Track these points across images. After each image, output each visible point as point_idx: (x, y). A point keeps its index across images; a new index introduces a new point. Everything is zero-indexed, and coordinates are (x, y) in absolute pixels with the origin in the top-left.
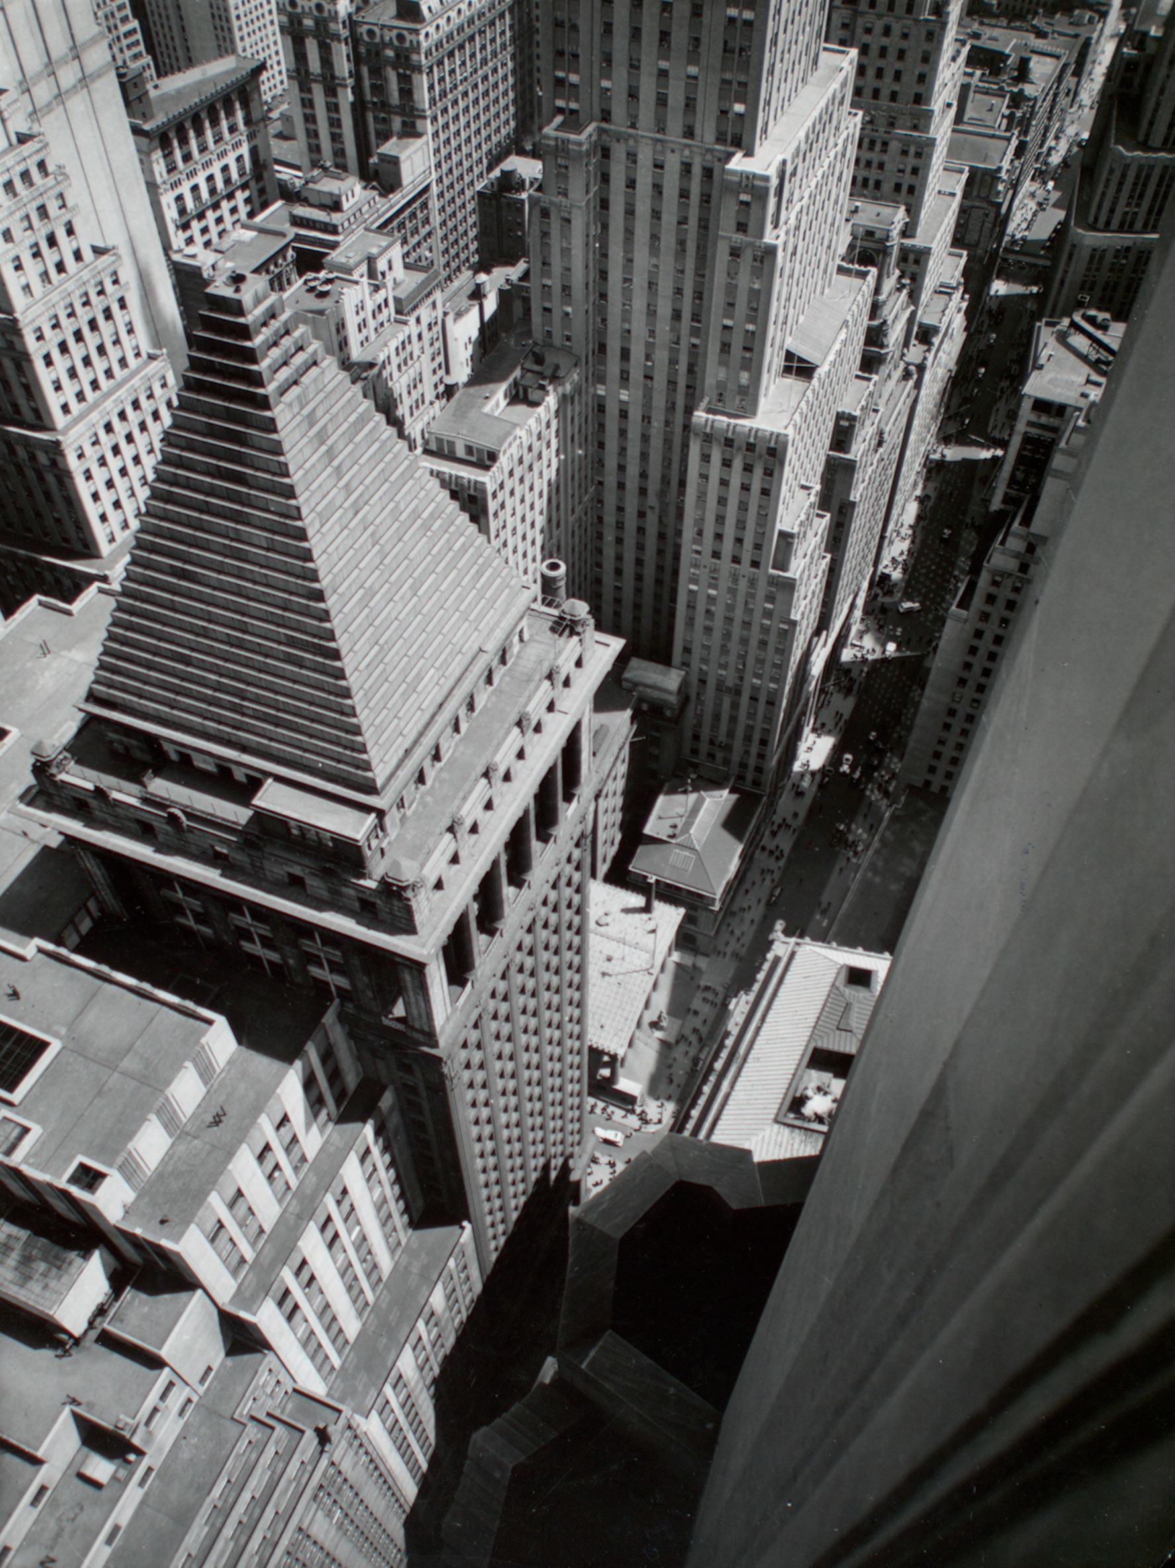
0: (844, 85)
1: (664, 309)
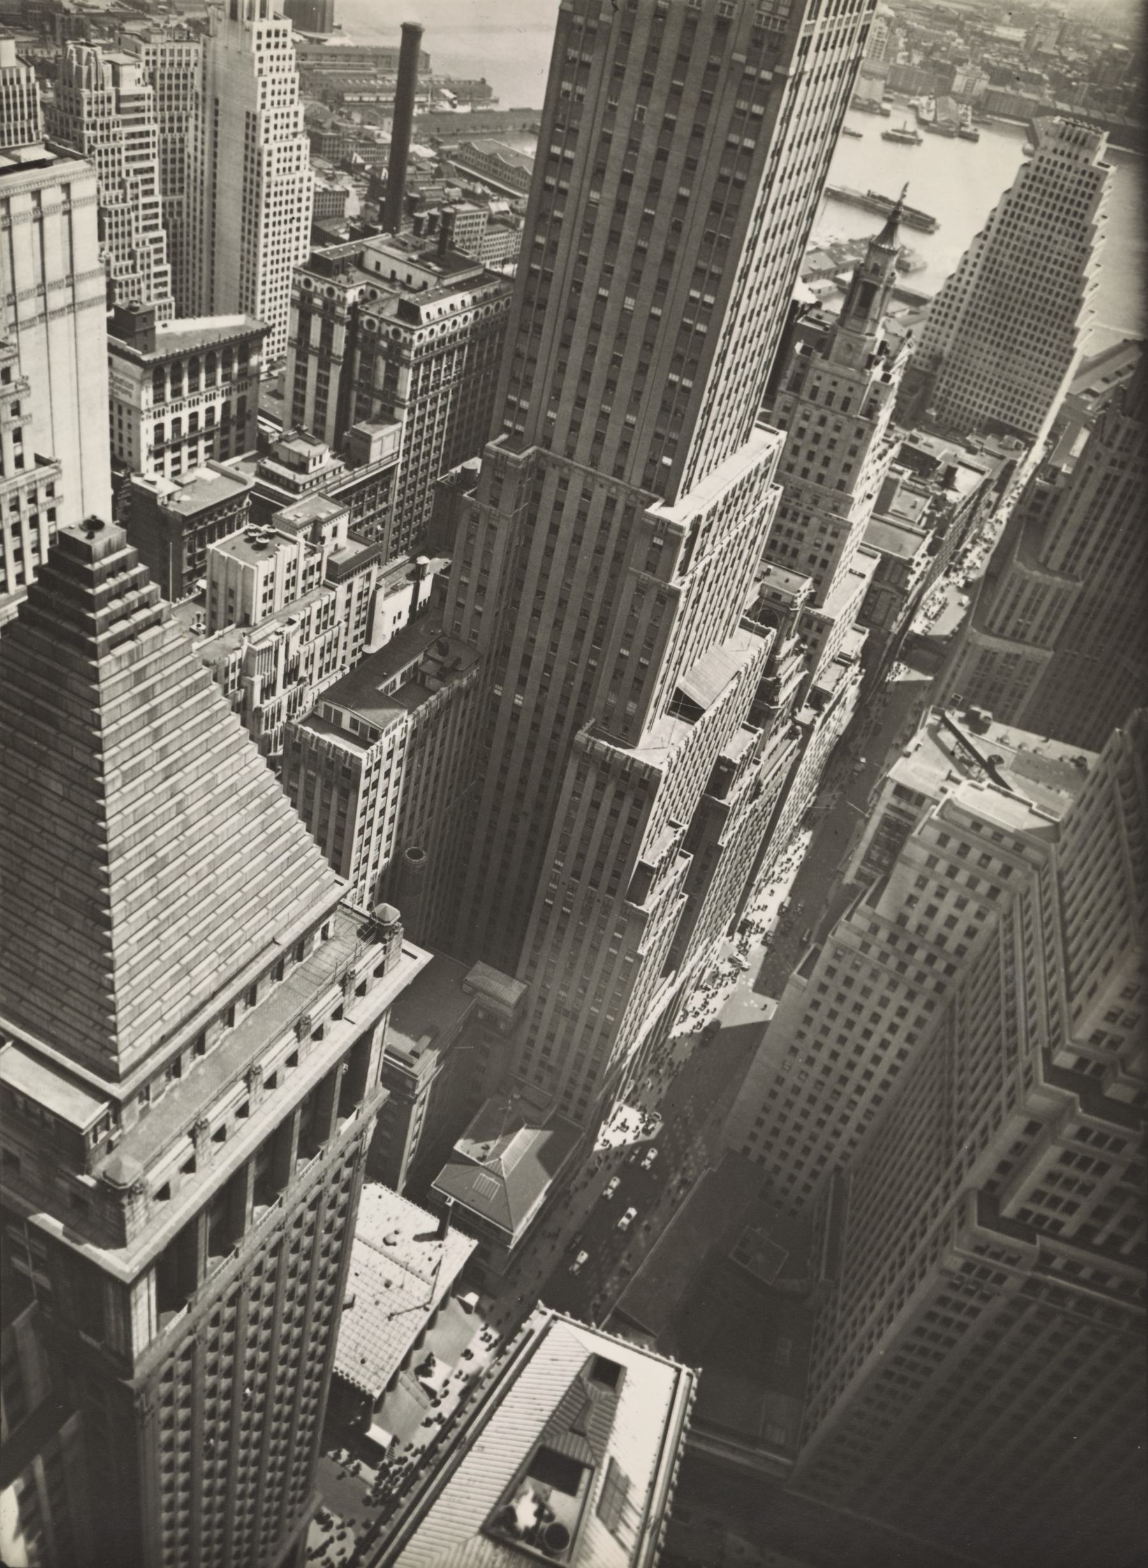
0: (769, 460)
1: (570, 626)
